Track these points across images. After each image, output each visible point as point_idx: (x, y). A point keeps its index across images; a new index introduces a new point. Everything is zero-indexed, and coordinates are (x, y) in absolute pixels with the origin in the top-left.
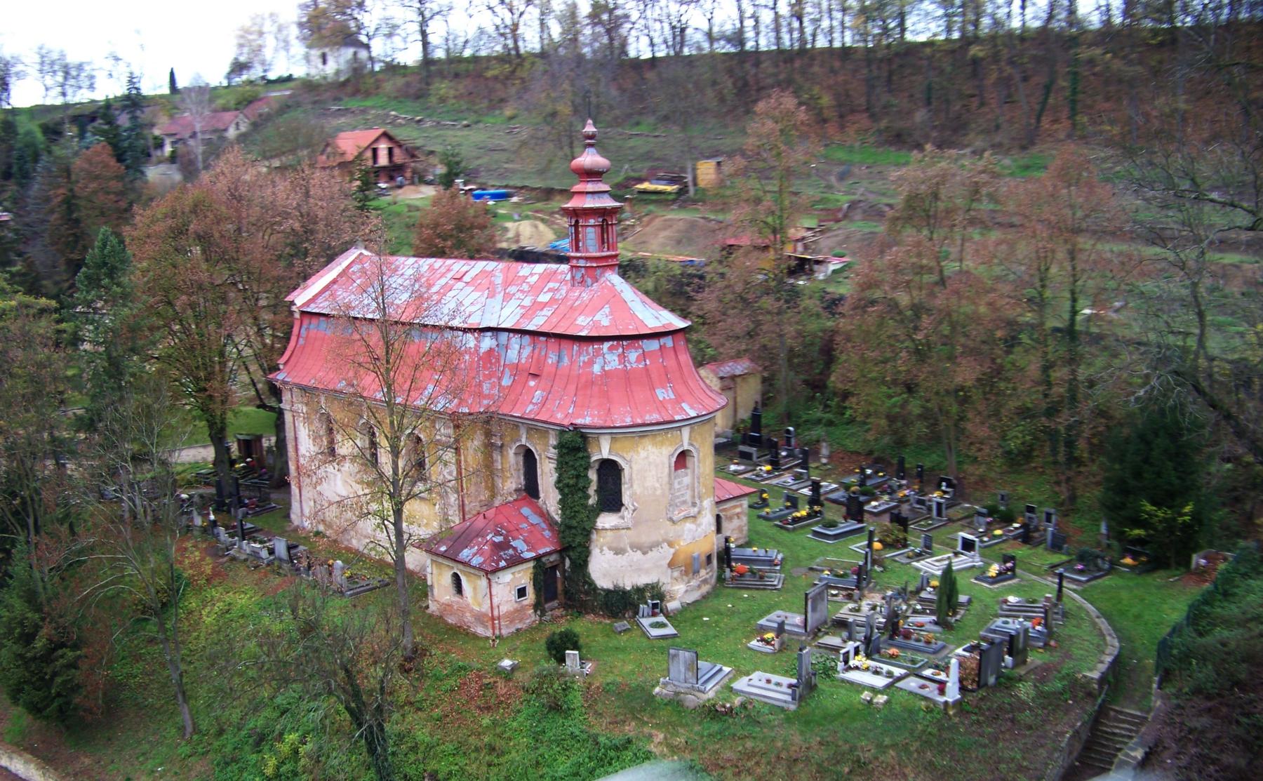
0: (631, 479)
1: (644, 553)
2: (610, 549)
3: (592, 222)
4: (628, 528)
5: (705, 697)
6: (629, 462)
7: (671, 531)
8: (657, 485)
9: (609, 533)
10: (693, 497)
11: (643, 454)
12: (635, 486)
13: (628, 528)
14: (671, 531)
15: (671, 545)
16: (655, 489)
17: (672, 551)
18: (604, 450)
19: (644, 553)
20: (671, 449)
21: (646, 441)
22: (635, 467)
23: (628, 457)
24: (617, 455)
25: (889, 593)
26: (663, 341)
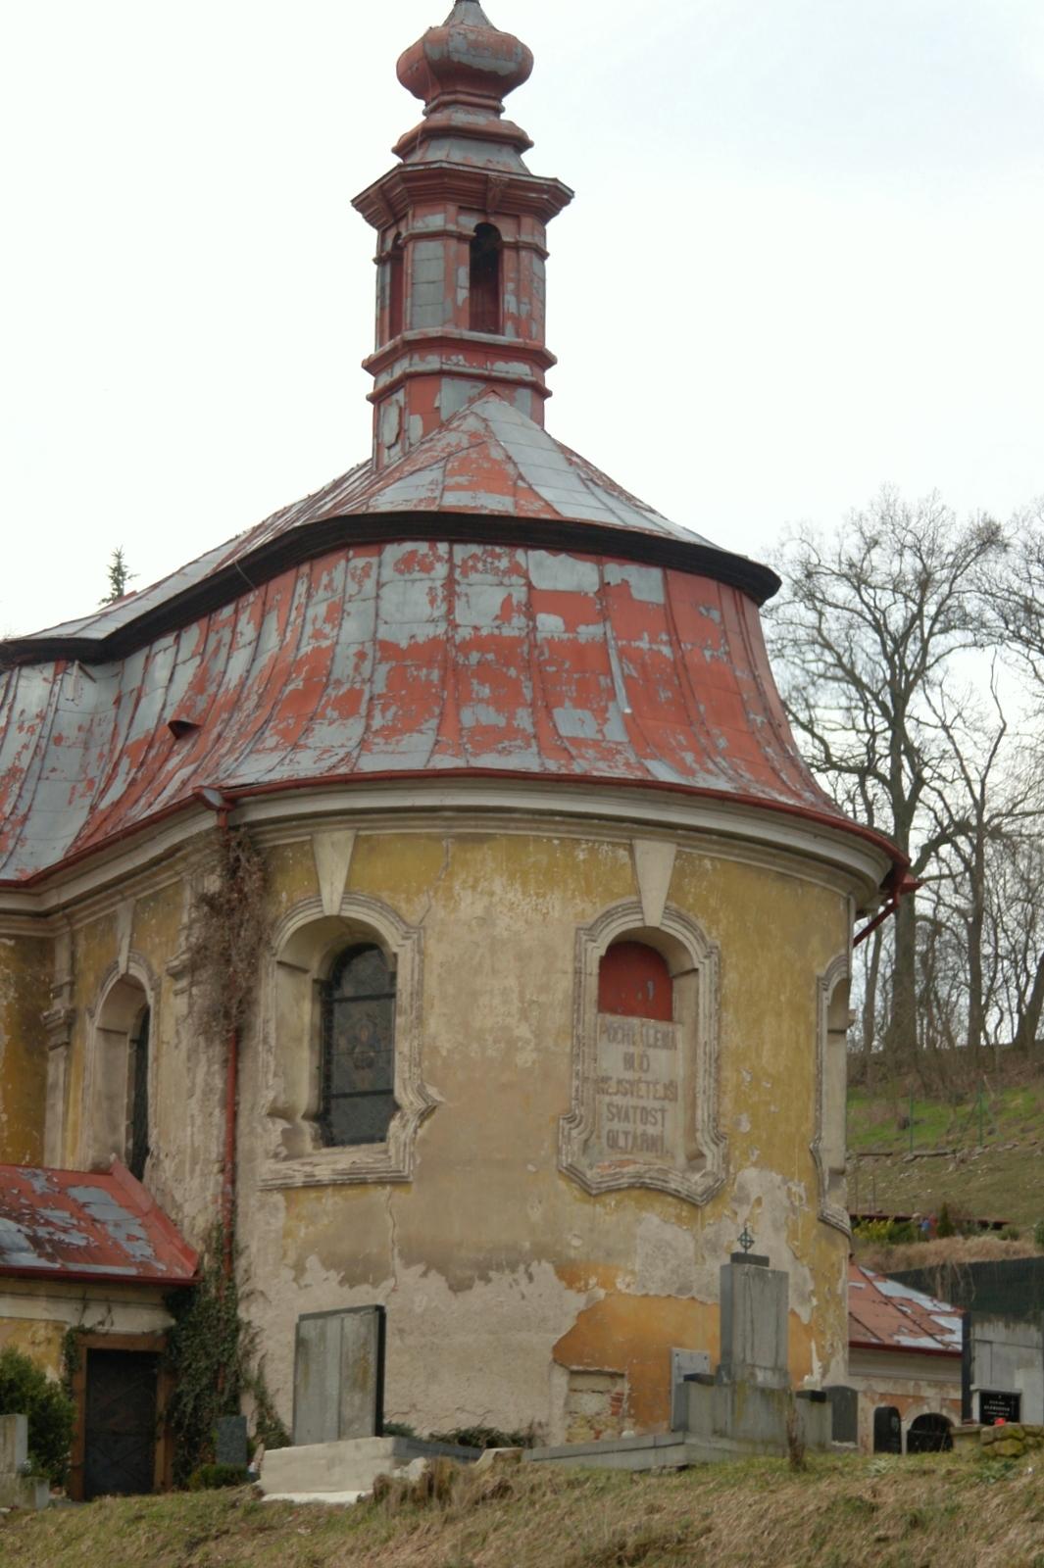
0: (418, 993)
1: (458, 1287)
2: (329, 1263)
3: (435, 221)
4: (399, 1182)
5: (62, 1014)
6: (415, 931)
7: (581, 1225)
8: (523, 1031)
9: (331, 1201)
10: (691, 1130)
11: (470, 905)
12: (434, 1024)
13: (399, 1182)
14: (581, 1225)
15: (570, 1274)
16: (512, 1045)
17: (576, 1302)
18: (331, 883)
19: (458, 1287)
20: (592, 910)
21: (486, 858)
22: (437, 951)
23: (413, 912)
24: (375, 902)
25: (723, 641)
26: (617, 572)
